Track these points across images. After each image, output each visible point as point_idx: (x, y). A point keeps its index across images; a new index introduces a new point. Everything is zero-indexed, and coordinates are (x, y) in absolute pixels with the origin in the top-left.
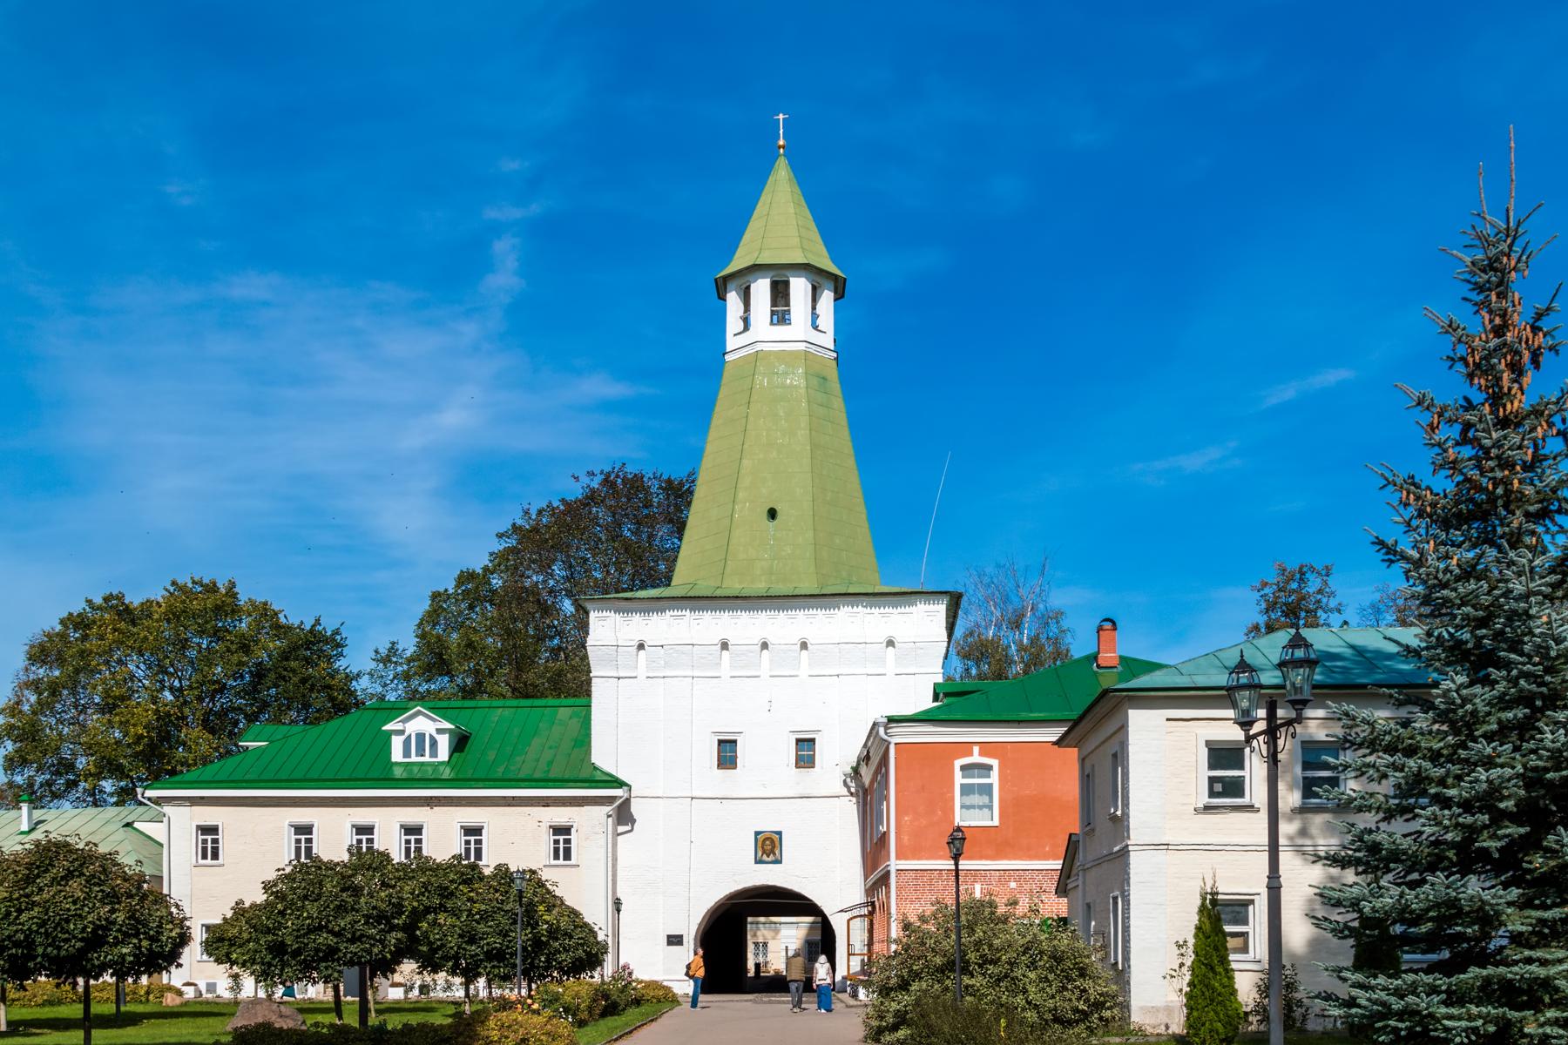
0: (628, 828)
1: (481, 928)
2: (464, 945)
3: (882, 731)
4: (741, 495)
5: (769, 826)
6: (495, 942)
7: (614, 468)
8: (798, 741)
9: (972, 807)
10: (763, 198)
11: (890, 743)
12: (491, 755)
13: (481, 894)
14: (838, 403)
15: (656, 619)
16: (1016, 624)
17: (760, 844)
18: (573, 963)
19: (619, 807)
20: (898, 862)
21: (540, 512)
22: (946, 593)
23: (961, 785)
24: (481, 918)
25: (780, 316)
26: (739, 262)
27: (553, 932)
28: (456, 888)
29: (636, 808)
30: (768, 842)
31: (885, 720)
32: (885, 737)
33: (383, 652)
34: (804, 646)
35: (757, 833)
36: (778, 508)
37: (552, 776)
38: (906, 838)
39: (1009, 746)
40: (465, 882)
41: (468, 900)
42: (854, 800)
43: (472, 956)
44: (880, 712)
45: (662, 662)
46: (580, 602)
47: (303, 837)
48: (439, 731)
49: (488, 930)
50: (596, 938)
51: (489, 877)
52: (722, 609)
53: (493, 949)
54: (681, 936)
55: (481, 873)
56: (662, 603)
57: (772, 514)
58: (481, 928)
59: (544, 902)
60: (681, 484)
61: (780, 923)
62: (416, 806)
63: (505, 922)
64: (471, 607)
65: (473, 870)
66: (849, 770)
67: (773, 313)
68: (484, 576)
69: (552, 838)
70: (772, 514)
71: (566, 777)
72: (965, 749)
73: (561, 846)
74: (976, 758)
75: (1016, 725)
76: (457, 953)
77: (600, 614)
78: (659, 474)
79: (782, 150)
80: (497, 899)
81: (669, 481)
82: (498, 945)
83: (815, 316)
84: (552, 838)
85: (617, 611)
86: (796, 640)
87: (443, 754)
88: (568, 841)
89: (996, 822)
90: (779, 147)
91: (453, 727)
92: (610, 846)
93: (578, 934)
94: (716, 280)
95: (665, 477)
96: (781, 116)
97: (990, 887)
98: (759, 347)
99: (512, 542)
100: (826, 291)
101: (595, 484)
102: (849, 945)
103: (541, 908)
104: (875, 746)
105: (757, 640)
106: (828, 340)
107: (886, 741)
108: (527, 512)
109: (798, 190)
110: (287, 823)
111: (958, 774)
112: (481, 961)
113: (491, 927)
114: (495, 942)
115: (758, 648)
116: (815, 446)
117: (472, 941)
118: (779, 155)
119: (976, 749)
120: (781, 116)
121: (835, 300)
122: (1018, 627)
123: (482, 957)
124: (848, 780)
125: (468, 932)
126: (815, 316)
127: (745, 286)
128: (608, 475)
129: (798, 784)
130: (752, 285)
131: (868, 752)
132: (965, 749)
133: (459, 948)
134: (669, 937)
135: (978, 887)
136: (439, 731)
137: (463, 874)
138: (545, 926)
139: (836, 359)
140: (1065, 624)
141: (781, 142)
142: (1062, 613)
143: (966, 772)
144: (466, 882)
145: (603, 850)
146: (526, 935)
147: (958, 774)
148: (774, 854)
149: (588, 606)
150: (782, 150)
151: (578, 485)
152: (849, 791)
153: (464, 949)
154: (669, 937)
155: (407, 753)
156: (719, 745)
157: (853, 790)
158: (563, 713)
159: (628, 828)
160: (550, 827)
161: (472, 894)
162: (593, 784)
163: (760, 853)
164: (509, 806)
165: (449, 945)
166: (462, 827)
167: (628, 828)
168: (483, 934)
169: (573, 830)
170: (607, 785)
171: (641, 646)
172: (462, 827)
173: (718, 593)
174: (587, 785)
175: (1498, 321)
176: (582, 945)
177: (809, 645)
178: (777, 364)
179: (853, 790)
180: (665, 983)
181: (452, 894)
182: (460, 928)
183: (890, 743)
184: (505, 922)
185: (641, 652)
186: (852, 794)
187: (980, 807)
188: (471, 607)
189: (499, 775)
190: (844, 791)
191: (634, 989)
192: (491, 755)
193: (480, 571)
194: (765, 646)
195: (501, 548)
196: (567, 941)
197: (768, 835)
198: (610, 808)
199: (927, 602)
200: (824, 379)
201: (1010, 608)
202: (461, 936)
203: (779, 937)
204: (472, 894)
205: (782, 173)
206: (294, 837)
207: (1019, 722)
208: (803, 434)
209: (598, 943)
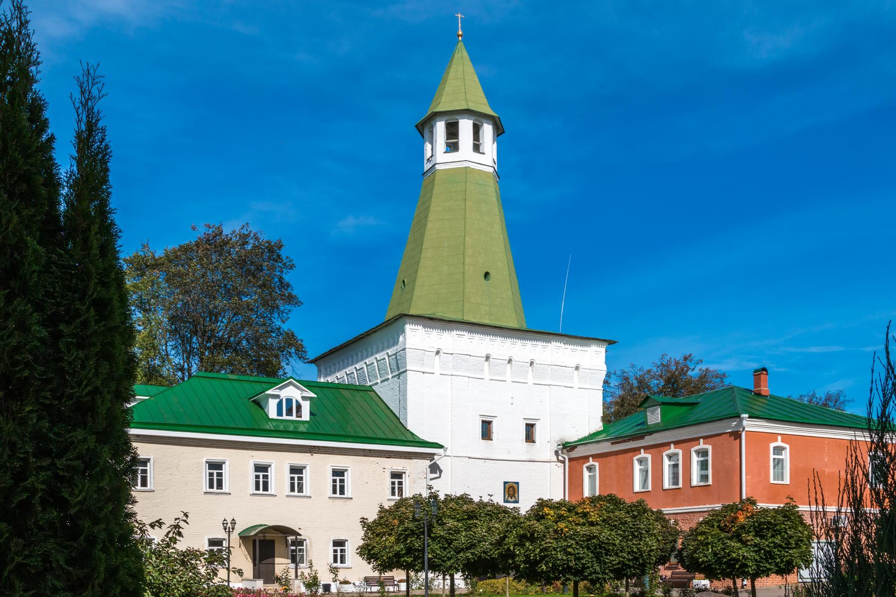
0: (437, 475)
4: (467, 260)
5: (512, 479)
17: (507, 489)
25: (453, 147)
30: (511, 489)
34: (532, 363)
35: (505, 483)
47: (215, 472)
48: (304, 398)
62: (301, 452)
70: (487, 275)
74: (779, 443)
75: (800, 424)
79: (460, 38)
87: (306, 416)
90: (459, 36)
110: (205, 460)
119: (779, 438)
129: (528, 452)
132: (773, 437)
136: (304, 398)
148: (515, 497)
149: (484, 122)
150: (460, 38)
155: (280, 413)
163: (507, 496)
164: (365, 456)
171: (438, 353)
194: (510, 361)
205: (462, 55)
206: (208, 471)
207: (802, 423)
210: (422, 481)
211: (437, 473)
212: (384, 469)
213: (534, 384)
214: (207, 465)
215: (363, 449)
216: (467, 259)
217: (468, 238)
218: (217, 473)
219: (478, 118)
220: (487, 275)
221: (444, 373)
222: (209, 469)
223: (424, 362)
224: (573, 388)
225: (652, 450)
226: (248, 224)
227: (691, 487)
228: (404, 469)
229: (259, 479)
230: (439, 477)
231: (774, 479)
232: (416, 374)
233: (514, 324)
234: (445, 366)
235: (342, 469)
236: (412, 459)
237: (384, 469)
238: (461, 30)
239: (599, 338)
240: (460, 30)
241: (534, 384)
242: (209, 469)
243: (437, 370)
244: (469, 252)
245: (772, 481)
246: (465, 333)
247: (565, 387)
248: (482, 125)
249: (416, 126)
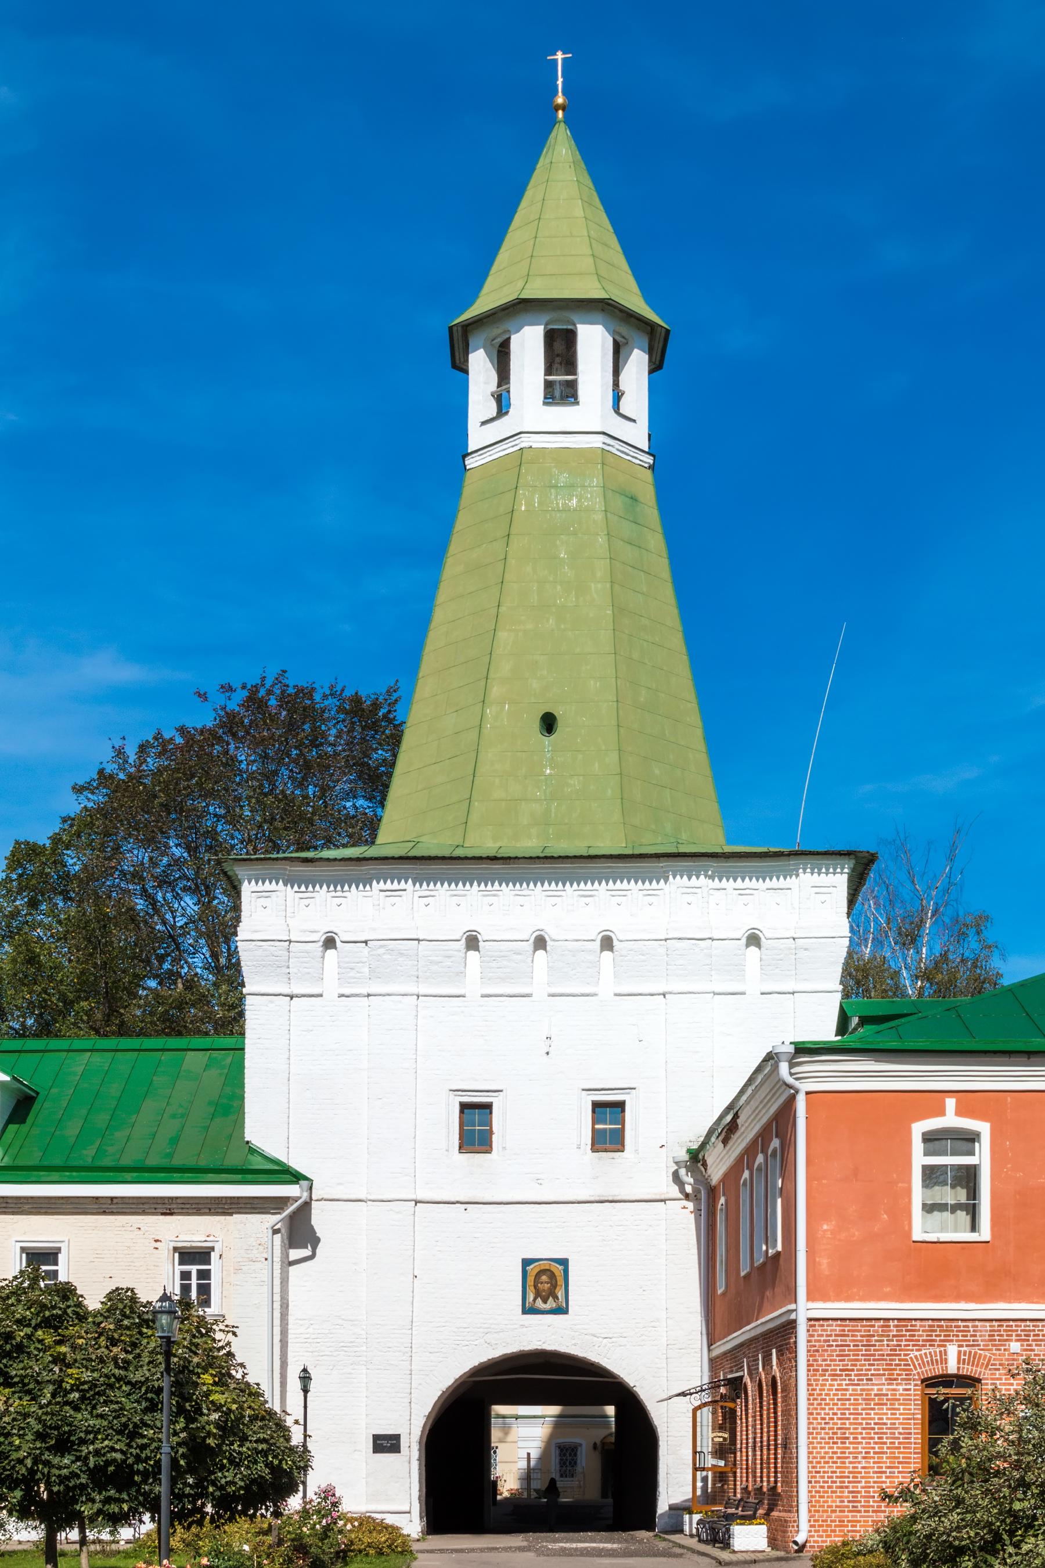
1: (83, 1419)
2: (46, 1456)
3: (784, 1068)
5: (544, 1250)
6: (113, 1449)
7: (263, 679)
8: (596, 1106)
9: (941, 1207)
10: (529, 194)
12: (72, 1130)
13: (81, 1348)
14: (656, 541)
15: (354, 895)
16: (910, 938)
18: (247, 1488)
19: (292, 1217)
20: (811, 1305)
21: (143, 748)
22: (848, 854)
23: (925, 1168)
24: (83, 1398)
26: (486, 302)
27: (230, 1428)
28: (29, 1337)
29: (320, 1219)
30: (544, 1278)
31: (791, 1049)
32: (790, 1080)
34: (607, 943)
35: (526, 1262)
36: (558, 712)
37: (177, 1161)
38: (824, 1262)
39: (1009, 1098)
40: (47, 1323)
41: (55, 1361)
42: (690, 1205)
43: (63, 1479)
44: (783, 1040)
45: (366, 970)
46: (226, 866)
49: (97, 1422)
50: (288, 1439)
51: (95, 1315)
52: (468, 879)
53: (108, 1463)
54: (397, 1437)
55: (79, 1305)
56: (365, 868)
57: (549, 723)
58: (83, 1419)
59: (211, 1365)
60: (376, 705)
61: (517, 1417)
63: (132, 1406)
64: (33, 904)
65: (65, 1298)
66: (684, 1156)
67: (548, 385)
68: (54, 850)
69: (179, 1268)
70: (549, 723)
71: (203, 1163)
73: (194, 1282)
74: (951, 1119)
76: (32, 1472)
77: (260, 887)
78: (339, 688)
80: (115, 1359)
81: (357, 700)
82: (118, 1456)
83: (618, 396)
84: (179, 1268)
85: (289, 881)
86: (594, 933)
88: (204, 1275)
89: (985, 1233)
90: (557, 108)
91: (7, 1078)
92: (277, 1282)
93: (256, 1432)
94: (451, 329)
95: (348, 693)
96: (560, 56)
98: (525, 441)
99: (99, 798)
100: (636, 352)
101: (233, 706)
102: (695, 1452)
103: (207, 1378)
104: (754, 1104)
105: (528, 933)
106: (638, 434)
107: (790, 1087)
108: (120, 752)
109: (587, 181)
111: (917, 1146)
112: (83, 1487)
113: (101, 1416)
114: (113, 1449)
115: (529, 946)
116: (620, 610)
117: (63, 1446)
118: (554, 122)
119: (951, 1103)
120: (560, 56)
121: (651, 372)
122: (913, 941)
123: (84, 1479)
124: (683, 1172)
125: (57, 1428)
126: (618, 396)
127: (499, 340)
128: (255, 690)
130: (513, 337)
131: (736, 1116)
133: (36, 1461)
134: (376, 1438)
135: (952, 1351)
137: (43, 1307)
138: (215, 1416)
139: (652, 467)
140: (990, 934)
141: (560, 100)
142: (987, 918)
143: (930, 1145)
144: (52, 1323)
145: (265, 1290)
146: (176, 1434)
147: (917, 1146)
148: (556, 1298)
149: (576, 321)
150: (560, 114)
151: (208, 706)
152: (682, 1190)
153: (47, 1463)
154: (376, 1438)
156: (462, 1112)
157: (689, 1189)
158: (194, 1060)
159: (306, 1252)
160: (175, 1249)
161: (63, 1349)
162: (250, 1177)
163: (531, 1297)
164: (104, 1213)
165: (14, 1456)
166: (23, 1249)
167: (306, 1252)
168: (87, 1432)
169: (214, 1256)
170: (273, 1177)
171: (330, 943)
172: (23, 1249)
173: (459, 853)
174: (239, 1177)
176: (265, 1453)
177: (615, 943)
178: (555, 471)
179: (689, 1189)
180: (390, 1520)
181: (20, 1348)
182: (39, 1420)
183: (797, 1091)
184: (132, 1406)
185: (331, 953)
186: (687, 1196)
187: (955, 1208)
188: (33, 904)
189: (88, 1161)
190: (674, 1191)
191: (340, 1532)
192: (72, 1130)
193: (48, 843)
194: (540, 943)
195: (78, 808)
196: (235, 1447)
197: (544, 1265)
198: (278, 1217)
199: (817, 869)
200: (634, 499)
201: (899, 911)
202: (40, 1436)
203: (510, 1438)
204: (63, 1349)
208: (598, 589)
209: (292, 1449)
210: (258, 1265)
211: (307, 1248)
212: (156, 1241)
213: (616, 995)
214: (177, 1255)
215: (93, 1197)
216: (495, 689)
217: (506, 634)
218: (198, 1271)
221: (347, 992)
222: (180, 1264)
223: (291, 970)
224: (744, 993)
225: (233, 1160)
226: (284, 672)
228: (211, 1238)
229: (190, 1280)
230: (312, 1257)
232: (272, 1002)
233: (717, 842)
234: (351, 974)
235: (51, 1248)
236: (231, 1214)
237: (156, 1241)
238: (564, 94)
239: (820, 850)
240: (560, 94)
241: (616, 995)
242: (180, 1264)
243: (331, 986)
244: (503, 668)
246: (273, 886)
247: (715, 994)
248: (576, 328)
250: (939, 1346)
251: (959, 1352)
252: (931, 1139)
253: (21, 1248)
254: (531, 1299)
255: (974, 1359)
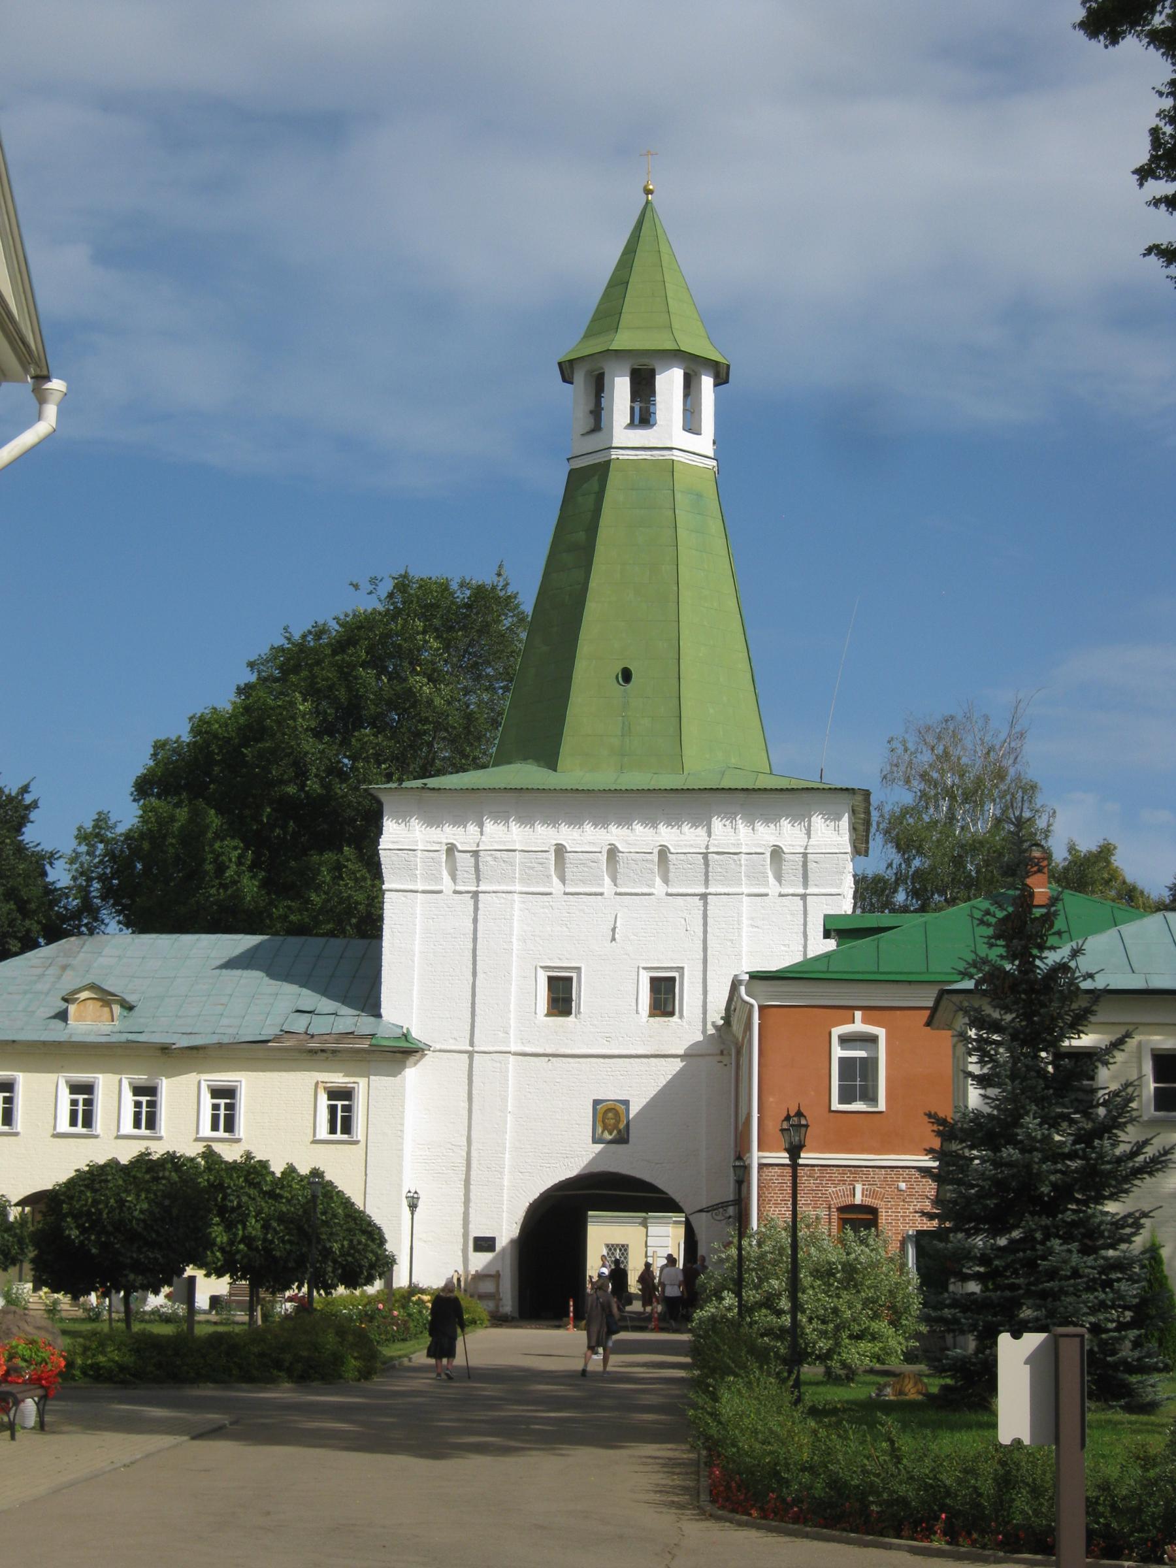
11: (752, 1006)
17: (600, 1116)
25: (643, 418)
30: (610, 1115)
33: (89, 825)
35: (596, 1102)
70: (627, 675)
72: (846, 1011)
74: (859, 1025)
89: (836, 1105)
97: (873, 1188)
119: (858, 1014)
143: (845, 1045)
163: (600, 1130)
175: (62, 954)
218: (226, 1104)
219: (694, 366)
220: (627, 675)
227: (830, 1111)
229: (84, 1110)
231: (842, 1100)
245: (836, 1105)
249: (560, 364)
250: (850, 1184)
251: (863, 1189)
252: (845, 1041)
253: (632, 425)
254: (600, 1131)
255: (874, 1195)
